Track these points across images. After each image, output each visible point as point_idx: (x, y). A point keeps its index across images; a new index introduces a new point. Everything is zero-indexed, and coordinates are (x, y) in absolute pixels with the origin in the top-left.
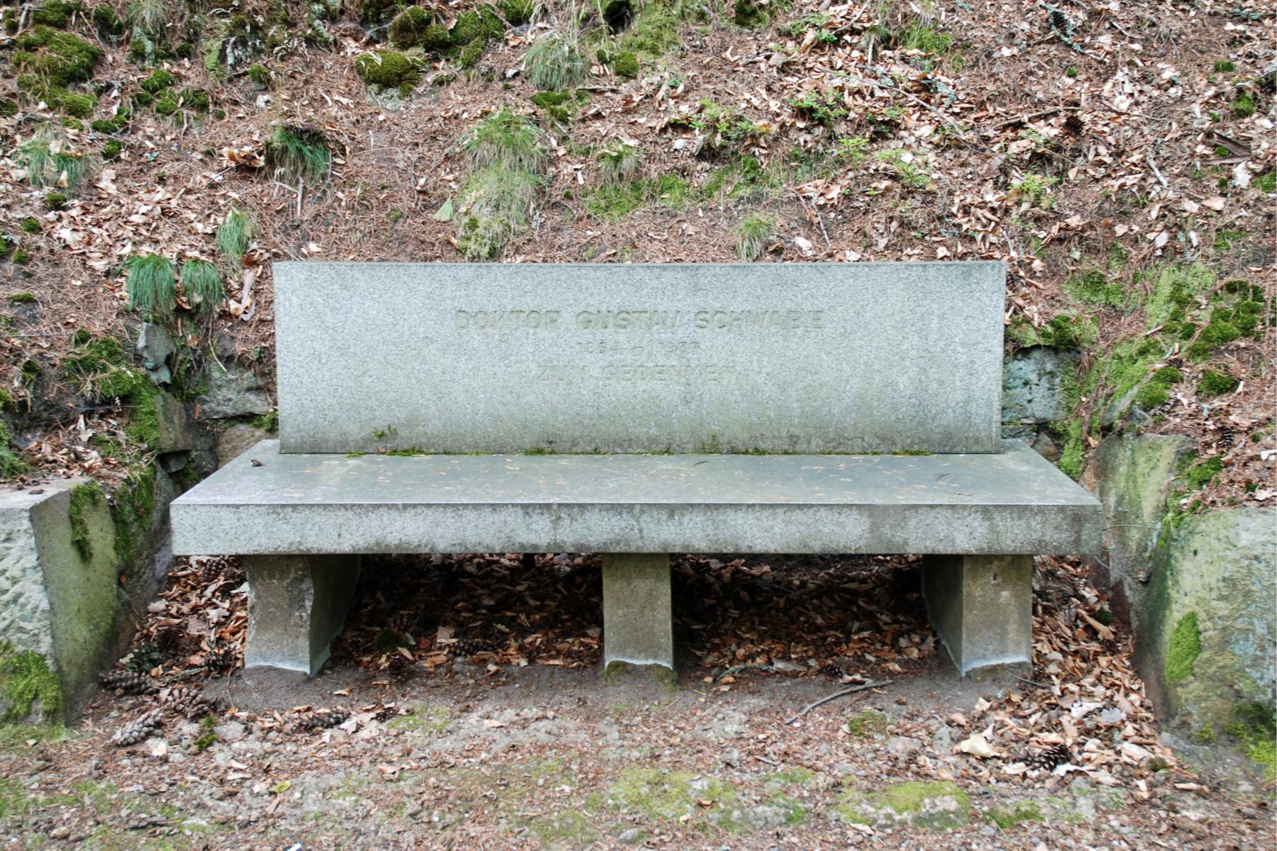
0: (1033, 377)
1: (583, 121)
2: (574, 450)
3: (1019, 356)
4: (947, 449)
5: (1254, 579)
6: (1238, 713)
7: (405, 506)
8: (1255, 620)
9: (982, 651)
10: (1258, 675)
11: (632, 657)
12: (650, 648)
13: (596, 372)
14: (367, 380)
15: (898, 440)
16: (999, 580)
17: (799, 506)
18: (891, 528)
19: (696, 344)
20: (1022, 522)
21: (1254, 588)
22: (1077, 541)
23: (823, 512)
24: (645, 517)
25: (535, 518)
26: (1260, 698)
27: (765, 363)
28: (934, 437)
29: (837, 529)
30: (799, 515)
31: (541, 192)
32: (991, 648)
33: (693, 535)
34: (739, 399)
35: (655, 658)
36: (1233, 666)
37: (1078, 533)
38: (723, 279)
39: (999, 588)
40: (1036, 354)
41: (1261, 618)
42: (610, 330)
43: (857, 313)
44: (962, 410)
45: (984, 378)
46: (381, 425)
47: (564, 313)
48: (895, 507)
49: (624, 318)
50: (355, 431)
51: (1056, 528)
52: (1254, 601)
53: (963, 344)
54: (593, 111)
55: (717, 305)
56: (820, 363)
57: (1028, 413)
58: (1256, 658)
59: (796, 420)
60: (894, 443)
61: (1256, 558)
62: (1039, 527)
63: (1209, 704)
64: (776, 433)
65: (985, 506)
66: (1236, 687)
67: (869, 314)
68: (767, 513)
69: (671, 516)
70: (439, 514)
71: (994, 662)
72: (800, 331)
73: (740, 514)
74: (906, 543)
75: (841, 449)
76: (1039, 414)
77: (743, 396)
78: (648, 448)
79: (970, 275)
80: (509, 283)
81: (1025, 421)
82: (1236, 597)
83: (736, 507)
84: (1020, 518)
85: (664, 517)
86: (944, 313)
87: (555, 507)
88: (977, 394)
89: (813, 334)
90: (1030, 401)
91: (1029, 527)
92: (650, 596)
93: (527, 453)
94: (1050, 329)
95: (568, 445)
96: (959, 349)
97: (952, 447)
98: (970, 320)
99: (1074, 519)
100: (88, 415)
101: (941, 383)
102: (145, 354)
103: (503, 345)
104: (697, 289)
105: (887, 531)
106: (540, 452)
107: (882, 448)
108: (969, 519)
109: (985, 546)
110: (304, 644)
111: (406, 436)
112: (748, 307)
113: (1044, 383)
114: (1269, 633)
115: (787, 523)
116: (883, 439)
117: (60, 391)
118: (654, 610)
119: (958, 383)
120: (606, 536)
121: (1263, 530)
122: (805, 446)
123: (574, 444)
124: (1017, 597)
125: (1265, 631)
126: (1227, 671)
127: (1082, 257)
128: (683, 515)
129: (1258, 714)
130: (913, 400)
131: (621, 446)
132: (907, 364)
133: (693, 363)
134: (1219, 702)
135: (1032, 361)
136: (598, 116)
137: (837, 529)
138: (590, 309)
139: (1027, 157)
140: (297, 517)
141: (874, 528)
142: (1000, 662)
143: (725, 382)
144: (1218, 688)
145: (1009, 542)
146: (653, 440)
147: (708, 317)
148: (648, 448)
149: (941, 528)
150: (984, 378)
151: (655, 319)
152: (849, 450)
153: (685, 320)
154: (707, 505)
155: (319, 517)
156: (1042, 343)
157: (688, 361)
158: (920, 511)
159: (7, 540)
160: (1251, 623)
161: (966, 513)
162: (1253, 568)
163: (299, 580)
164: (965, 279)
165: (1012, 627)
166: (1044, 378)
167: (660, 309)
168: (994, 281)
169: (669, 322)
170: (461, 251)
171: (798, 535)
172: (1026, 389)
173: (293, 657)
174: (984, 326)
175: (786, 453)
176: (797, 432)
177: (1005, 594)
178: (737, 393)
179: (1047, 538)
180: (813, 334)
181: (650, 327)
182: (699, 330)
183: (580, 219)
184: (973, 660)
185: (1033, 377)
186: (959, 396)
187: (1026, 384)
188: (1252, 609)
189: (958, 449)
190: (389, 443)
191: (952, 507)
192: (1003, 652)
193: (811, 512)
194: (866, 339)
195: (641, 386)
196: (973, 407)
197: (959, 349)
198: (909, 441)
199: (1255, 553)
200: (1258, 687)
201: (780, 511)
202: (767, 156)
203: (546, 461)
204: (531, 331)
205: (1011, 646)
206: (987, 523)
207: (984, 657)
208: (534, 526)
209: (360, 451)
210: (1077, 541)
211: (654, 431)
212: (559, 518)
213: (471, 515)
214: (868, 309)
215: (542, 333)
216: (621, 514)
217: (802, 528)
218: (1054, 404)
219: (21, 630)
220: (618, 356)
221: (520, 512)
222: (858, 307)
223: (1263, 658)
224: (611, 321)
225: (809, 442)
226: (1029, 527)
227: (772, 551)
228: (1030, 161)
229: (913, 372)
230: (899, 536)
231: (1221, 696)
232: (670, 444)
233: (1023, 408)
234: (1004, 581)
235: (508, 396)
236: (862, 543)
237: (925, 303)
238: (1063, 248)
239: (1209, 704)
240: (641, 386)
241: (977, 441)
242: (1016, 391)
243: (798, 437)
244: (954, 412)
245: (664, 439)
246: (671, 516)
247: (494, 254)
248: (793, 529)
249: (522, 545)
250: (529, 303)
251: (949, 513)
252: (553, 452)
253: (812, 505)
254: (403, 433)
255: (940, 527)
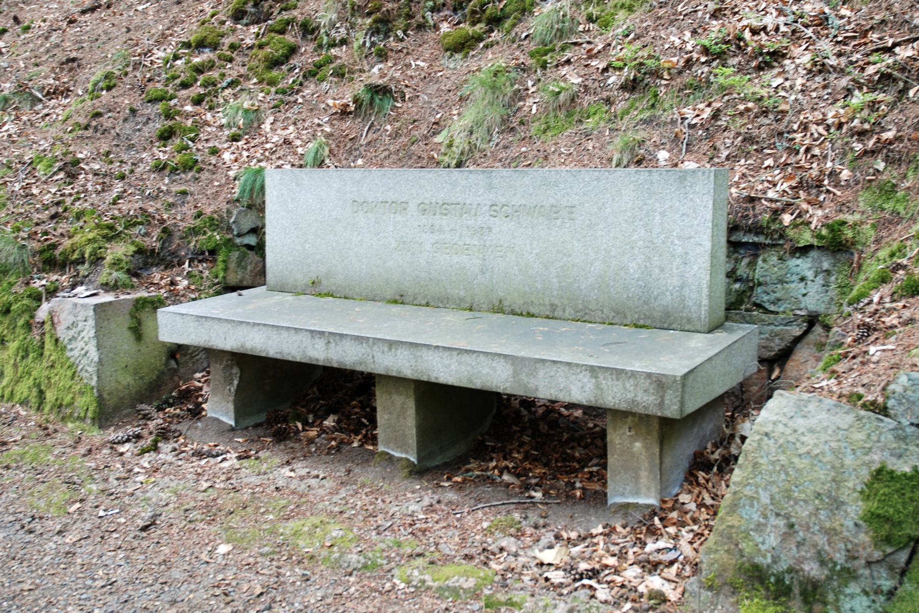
0: (810, 274)
1: (557, 66)
2: (415, 302)
3: (798, 255)
4: (666, 325)
5: (762, 454)
6: (740, 569)
7: (254, 324)
8: (760, 490)
9: (621, 489)
10: (761, 540)
11: (393, 450)
12: (403, 447)
13: (428, 246)
14: (307, 246)
15: (628, 315)
16: (633, 433)
17: (467, 351)
18: (527, 376)
19: (490, 229)
20: (619, 383)
21: (761, 461)
22: (661, 404)
23: (482, 358)
24: (375, 348)
25: (317, 340)
26: (759, 560)
27: (534, 246)
28: (655, 314)
29: (491, 372)
30: (466, 358)
31: (504, 121)
32: (628, 488)
33: (447, 371)
34: (517, 272)
35: (407, 453)
36: (739, 527)
37: (662, 397)
38: (508, 180)
39: (633, 439)
40: (814, 254)
41: (765, 489)
42: (437, 217)
43: (600, 209)
44: (678, 294)
45: (695, 268)
46: (313, 276)
47: (411, 204)
48: (530, 359)
49: (444, 208)
50: (302, 279)
51: (645, 391)
52: (760, 473)
53: (679, 238)
54: (565, 58)
55: (503, 200)
56: (566, 247)
57: (802, 306)
58: (759, 525)
59: (555, 292)
60: (625, 317)
61: (767, 434)
62: (632, 388)
63: (717, 556)
64: (541, 301)
65: (592, 367)
66: (740, 546)
67: (608, 210)
68: (447, 353)
69: (390, 349)
70: (269, 331)
71: (630, 500)
72: (559, 222)
73: (431, 352)
74: (537, 389)
75: (586, 318)
76: (812, 308)
77: (520, 270)
78: (459, 305)
79: (685, 179)
80: (468, 185)
81: (798, 312)
82: (747, 468)
83: (428, 346)
84: (618, 379)
85: (386, 349)
86: (665, 211)
87: (371, 341)
88: (690, 281)
89: (568, 225)
90: (804, 295)
91: (624, 387)
92: (403, 410)
93: (389, 302)
94: (824, 232)
95: (412, 298)
96: (676, 242)
97: (670, 324)
98: (685, 217)
99: (658, 385)
100: (191, 261)
101: (662, 270)
102: (233, 226)
103: (377, 225)
104: (490, 187)
105: (523, 377)
106: (395, 302)
107: (616, 320)
108: (581, 376)
109: (593, 399)
110: (231, 407)
111: (326, 285)
112: (524, 202)
113: (820, 280)
114: (772, 504)
115: (460, 363)
116: (617, 313)
117: (179, 245)
118: (405, 418)
119: (675, 271)
120: (354, 358)
121: (777, 410)
122: (561, 313)
123: (415, 299)
124: (647, 448)
125: (768, 501)
126: (734, 530)
127: (885, 168)
128: (397, 349)
129: (756, 574)
130: (640, 283)
131: (442, 302)
132: (636, 252)
133: (488, 243)
134: (725, 557)
135: (810, 260)
136: (568, 62)
137: (491, 372)
138: (426, 201)
139: (876, 78)
140: (208, 324)
141: (516, 374)
142: (635, 501)
143: (508, 259)
144: (726, 544)
145: (610, 398)
146: (462, 300)
147: (498, 208)
148: (459, 305)
149: (561, 381)
150: (695, 268)
151: (464, 210)
152: (592, 320)
153: (483, 211)
154: (411, 343)
155: (217, 326)
156: (816, 244)
157: (485, 241)
158: (547, 365)
159: (85, 321)
160: (757, 492)
161: (578, 371)
162: (763, 443)
163: (231, 367)
164: (681, 183)
165: (644, 474)
166: (821, 276)
167: (468, 202)
168: (704, 185)
169: (473, 212)
170: (438, 163)
171: (466, 373)
172: (802, 285)
173: (226, 414)
174: (696, 223)
175: (548, 317)
176: (556, 302)
177: (638, 445)
178: (515, 268)
179: (638, 399)
180: (568, 225)
181: (461, 216)
182: (492, 219)
183: (524, 139)
184: (615, 496)
185: (810, 274)
186: (676, 281)
187: (802, 279)
188: (758, 479)
189: (674, 326)
190: (316, 288)
191: (568, 364)
192: (637, 493)
193: (475, 355)
194: (606, 230)
195: (456, 259)
196: (686, 291)
197: (676, 242)
198: (636, 316)
199: (766, 430)
200: (759, 550)
201: (455, 353)
202: (667, 86)
203: (396, 309)
204: (392, 216)
205: (643, 490)
206: (594, 381)
207: (623, 495)
208: (316, 346)
209: (296, 292)
210: (661, 404)
211: (462, 293)
212: (329, 342)
213: (285, 334)
214: (607, 206)
215: (399, 218)
216: (362, 343)
217: (469, 368)
218: (827, 299)
219: (87, 371)
220: (442, 236)
221: (309, 335)
222: (600, 204)
223: (765, 525)
224: (438, 211)
225: (564, 311)
226: (624, 387)
227: (450, 383)
228: (879, 81)
229: (640, 259)
230: (532, 383)
231: (728, 551)
232: (472, 304)
233: (798, 301)
234: (637, 434)
235: (379, 261)
236: (507, 385)
237: (650, 202)
238: (871, 160)
239: (717, 556)
240: (456, 259)
241: (689, 321)
242: (793, 286)
243: (557, 306)
244: (672, 295)
245: (468, 299)
246: (390, 349)
247: (459, 165)
248: (463, 368)
249: (310, 358)
250: (391, 196)
251: (566, 369)
252: (402, 303)
253: (475, 352)
254: (324, 282)
255: (561, 380)
